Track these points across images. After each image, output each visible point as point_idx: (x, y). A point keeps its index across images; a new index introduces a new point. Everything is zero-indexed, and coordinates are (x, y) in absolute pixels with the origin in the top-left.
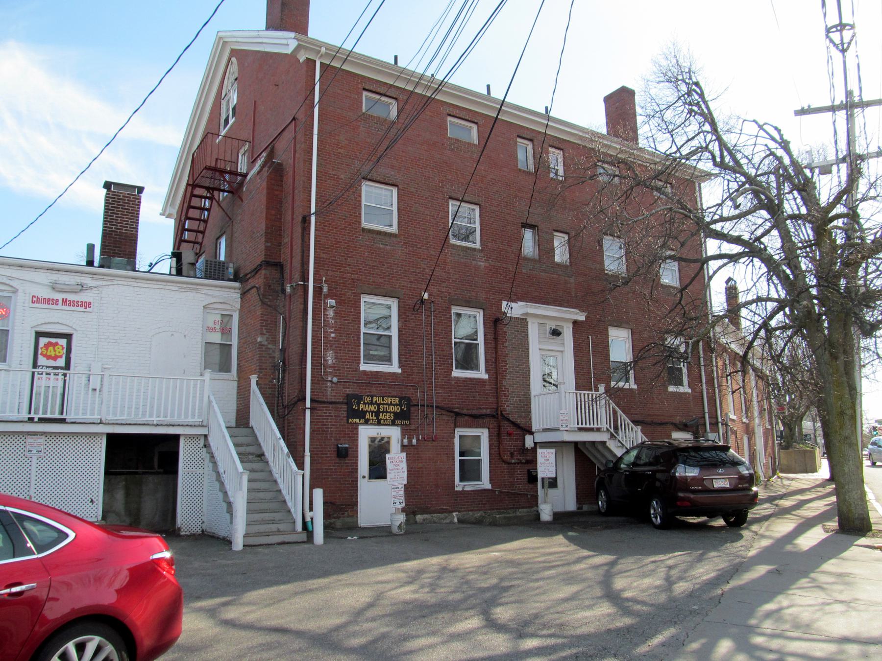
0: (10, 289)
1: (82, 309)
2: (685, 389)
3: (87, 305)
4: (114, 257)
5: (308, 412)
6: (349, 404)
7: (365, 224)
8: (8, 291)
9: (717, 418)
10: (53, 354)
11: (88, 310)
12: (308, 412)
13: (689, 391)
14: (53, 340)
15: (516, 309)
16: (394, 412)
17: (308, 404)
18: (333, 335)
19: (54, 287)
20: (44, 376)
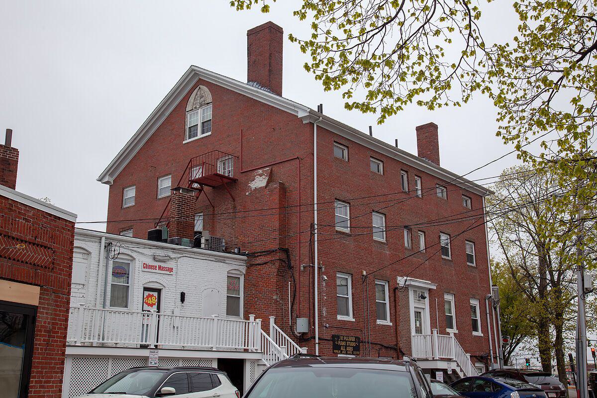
0: (85, 252)
1: (168, 273)
2: (388, 322)
3: (171, 270)
4: (183, 238)
5: (317, 346)
6: (333, 341)
7: (375, 238)
8: (128, 260)
9: (496, 354)
10: (150, 302)
11: (171, 273)
12: (317, 346)
13: (482, 335)
14: (151, 293)
15: (401, 281)
16: (353, 346)
17: (317, 341)
18: (325, 298)
19: (155, 259)
20: (226, 321)
